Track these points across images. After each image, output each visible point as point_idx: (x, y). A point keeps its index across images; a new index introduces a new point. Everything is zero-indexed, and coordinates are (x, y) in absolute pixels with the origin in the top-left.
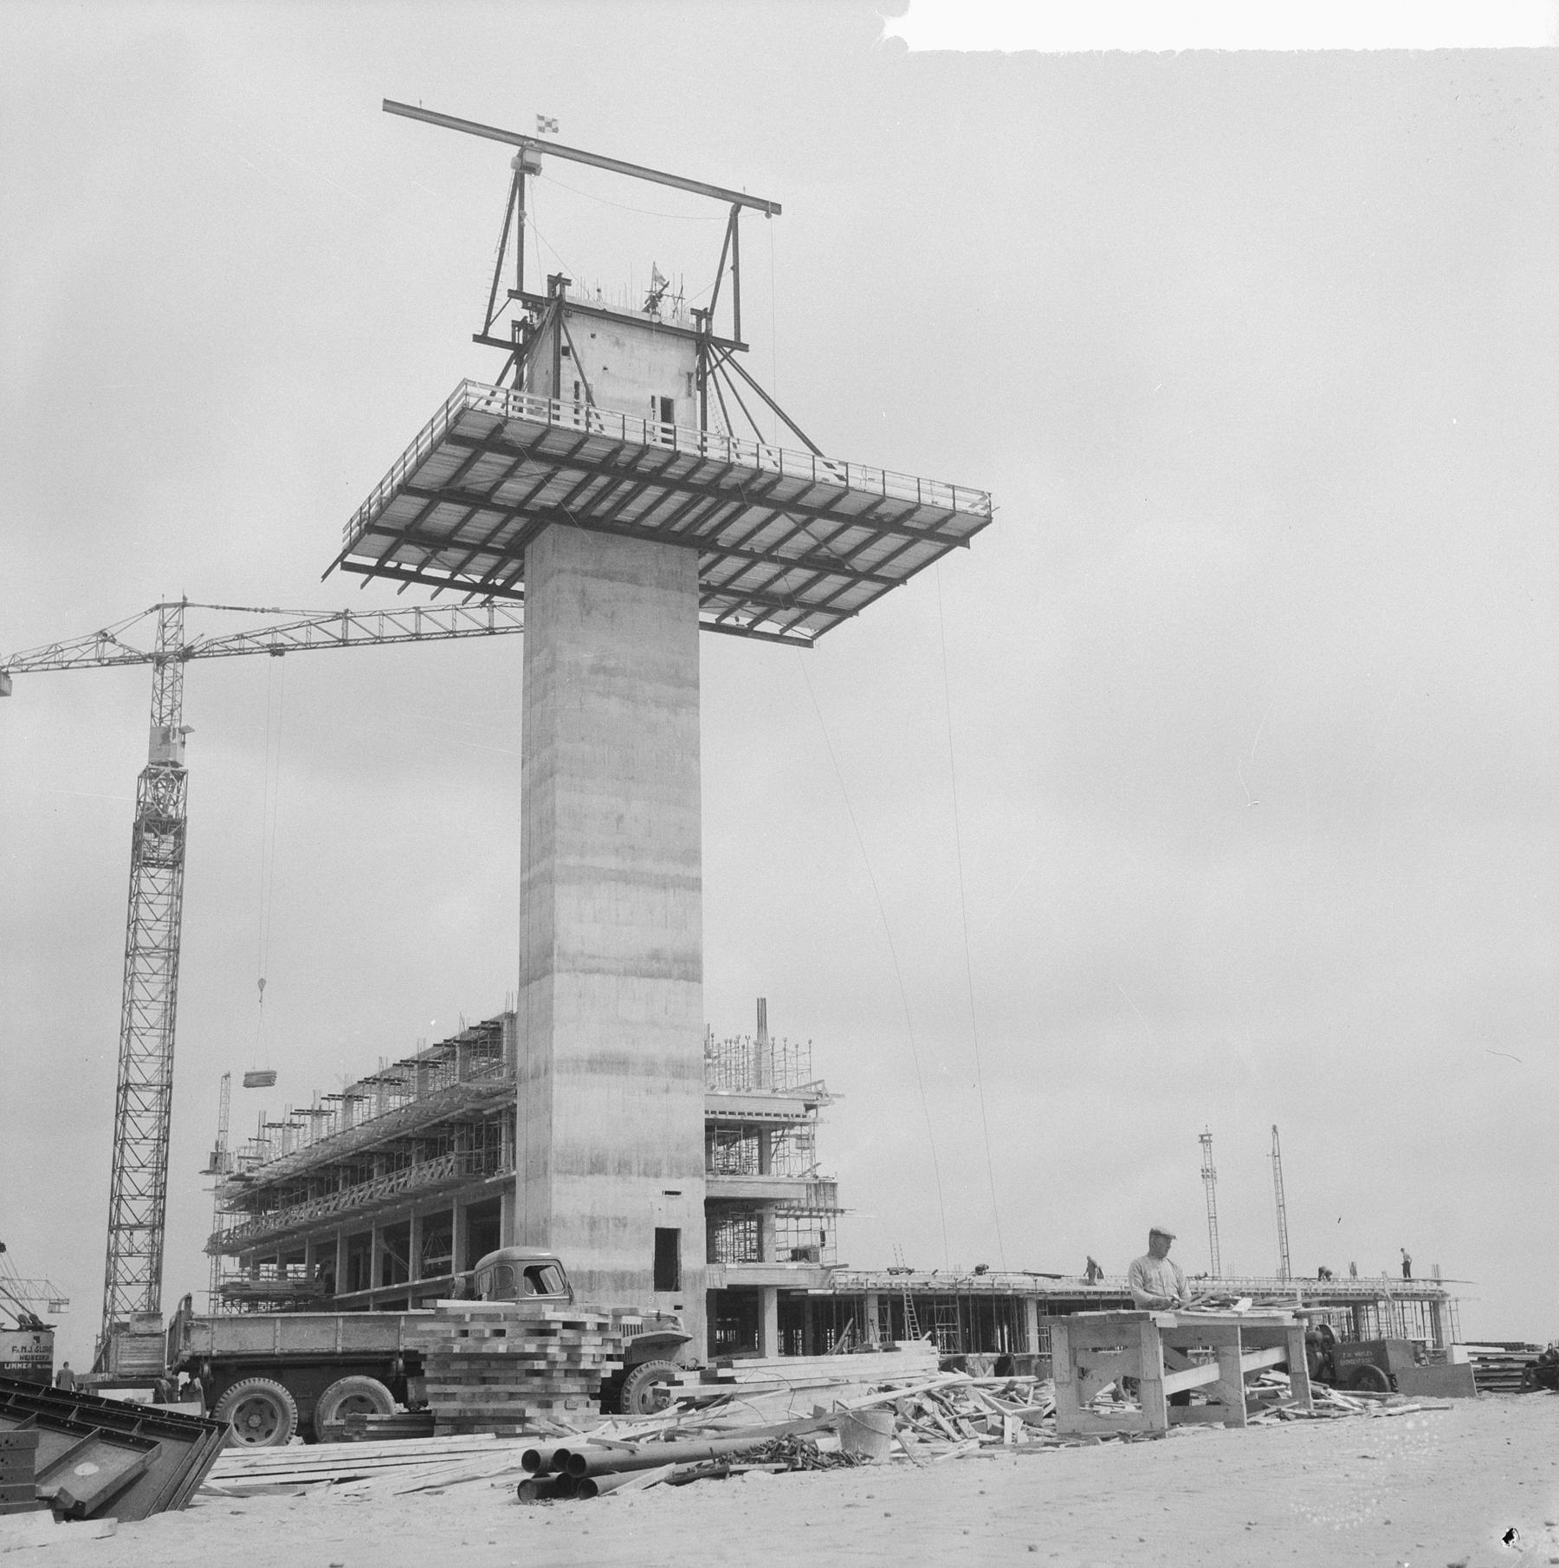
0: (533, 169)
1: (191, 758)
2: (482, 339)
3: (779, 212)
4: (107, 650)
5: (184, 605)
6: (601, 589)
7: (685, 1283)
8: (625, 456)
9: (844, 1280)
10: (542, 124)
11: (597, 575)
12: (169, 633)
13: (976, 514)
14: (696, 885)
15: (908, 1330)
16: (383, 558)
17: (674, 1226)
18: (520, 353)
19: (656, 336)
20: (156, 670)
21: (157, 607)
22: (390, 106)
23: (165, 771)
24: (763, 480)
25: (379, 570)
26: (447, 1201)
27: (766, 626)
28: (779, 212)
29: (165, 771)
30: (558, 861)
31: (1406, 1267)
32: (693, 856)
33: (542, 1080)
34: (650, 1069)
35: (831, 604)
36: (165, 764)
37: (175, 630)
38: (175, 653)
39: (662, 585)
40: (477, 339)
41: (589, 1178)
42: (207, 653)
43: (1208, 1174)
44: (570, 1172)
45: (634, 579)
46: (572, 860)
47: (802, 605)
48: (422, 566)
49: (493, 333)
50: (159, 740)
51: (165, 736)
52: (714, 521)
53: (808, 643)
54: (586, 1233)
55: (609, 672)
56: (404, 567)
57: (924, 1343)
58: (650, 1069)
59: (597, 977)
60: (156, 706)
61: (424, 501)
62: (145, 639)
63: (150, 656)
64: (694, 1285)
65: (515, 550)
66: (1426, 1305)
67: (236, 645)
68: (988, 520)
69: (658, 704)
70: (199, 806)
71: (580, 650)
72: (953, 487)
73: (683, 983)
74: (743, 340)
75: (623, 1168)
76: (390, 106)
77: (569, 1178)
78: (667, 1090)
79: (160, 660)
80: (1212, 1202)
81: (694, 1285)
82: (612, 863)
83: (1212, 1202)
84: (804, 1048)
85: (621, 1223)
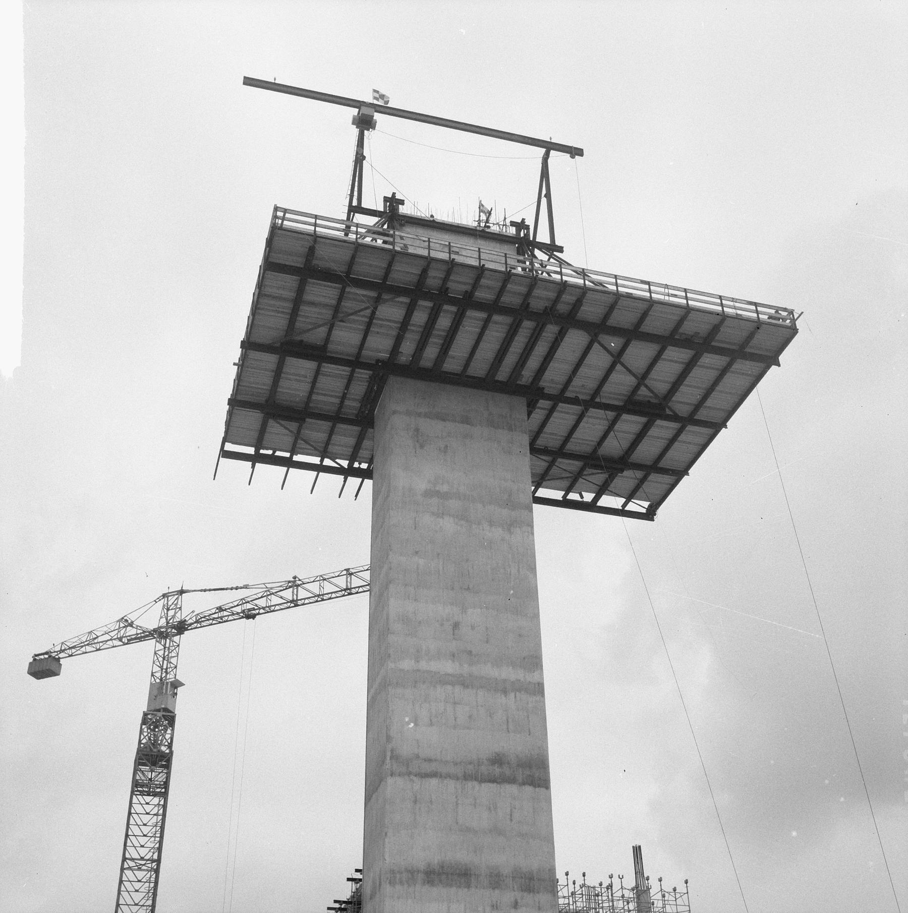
1: (182, 706)
3: (582, 155)
4: (129, 634)
8: (434, 279)
10: (377, 96)
11: (427, 416)
12: (171, 613)
15: (533, 677)
22: (249, 82)
23: (159, 717)
24: (569, 297)
27: (606, 501)
28: (582, 155)
29: (159, 717)
32: (534, 662)
34: (496, 880)
36: (159, 710)
39: (492, 424)
45: (466, 420)
46: (407, 664)
47: (637, 466)
48: (293, 452)
52: (533, 363)
55: (444, 496)
56: (278, 453)
57: (561, 312)
58: (496, 880)
59: (434, 781)
61: (599, 504)
62: (153, 620)
65: (366, 420)
69: (491, 523)
70: (184, 742)
73: (528, 789)
74: (558, 243)
79: (160, 634)
82: (448, 667)
84: (681, 888)
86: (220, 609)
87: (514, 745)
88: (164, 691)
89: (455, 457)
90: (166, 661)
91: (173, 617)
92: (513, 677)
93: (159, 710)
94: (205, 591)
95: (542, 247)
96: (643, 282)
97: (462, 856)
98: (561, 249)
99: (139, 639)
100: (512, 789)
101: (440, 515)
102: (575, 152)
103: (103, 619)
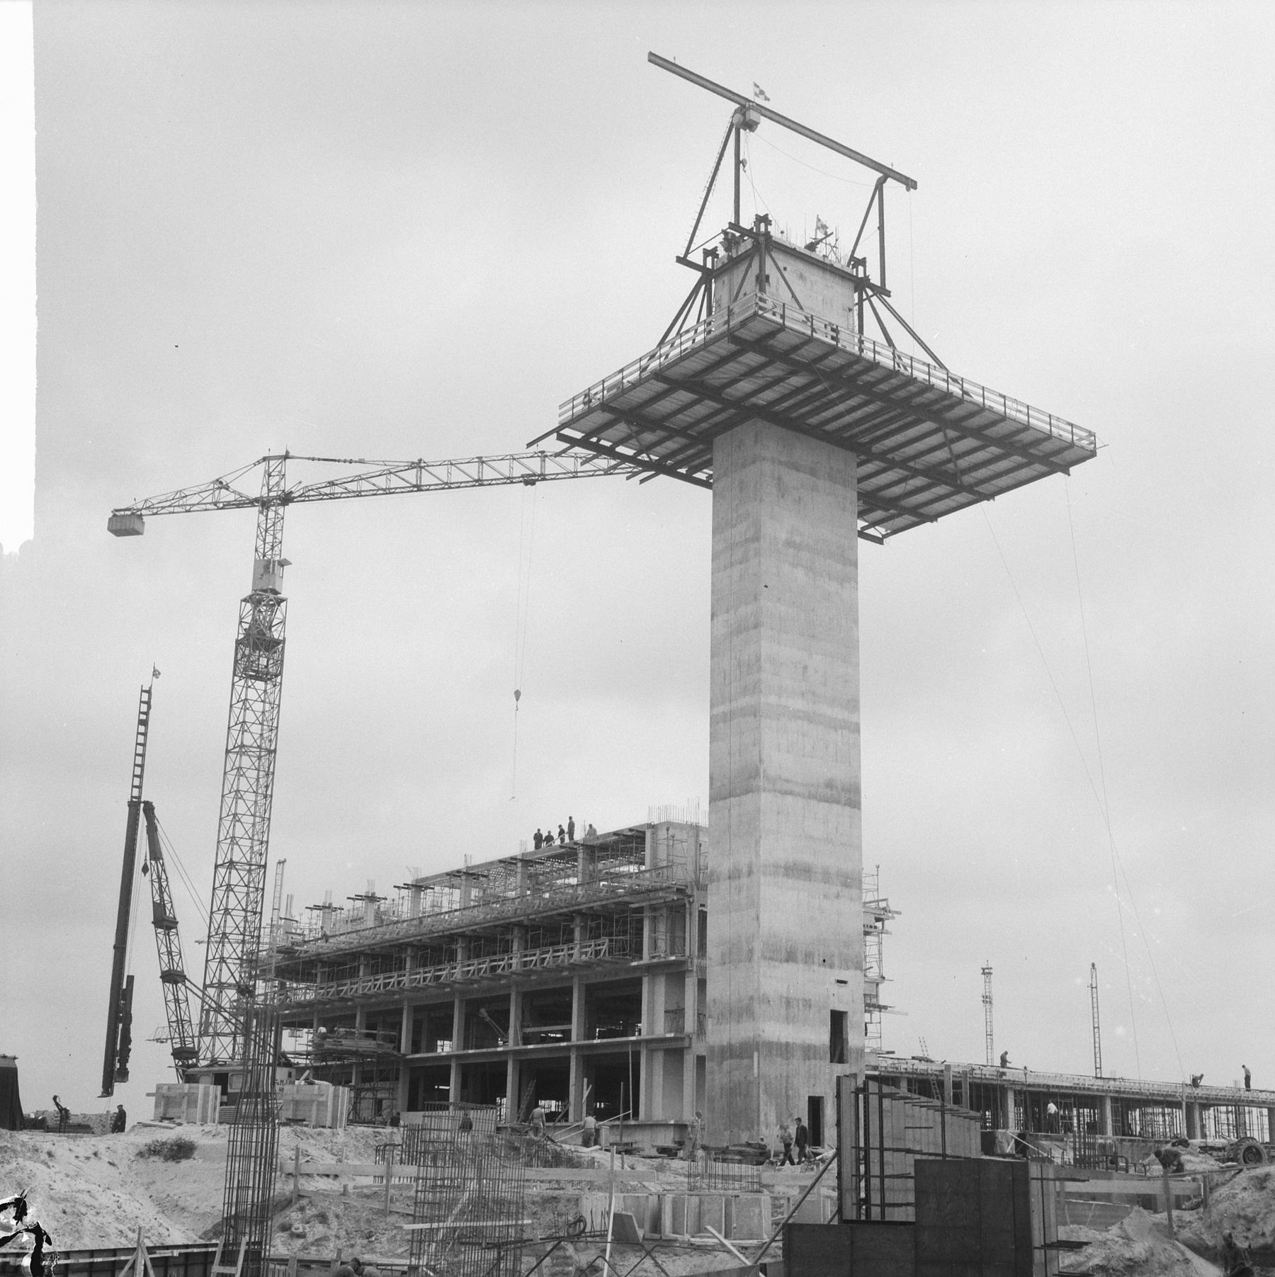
0: (751, 126)
1: (288, 585)
2: (682, 260)
3: (915, 188)
5: (286, 457)
6: (791, 477)
7: (851, 1057)
9: (884, 1064)
12: (273, 481)
13: (1082, 448)
14: (856, 729)
15: (854, 718)
16: (589, 435)
17: (842, 1009)
18: (708, 276)
19: (828, 276)
20: (261, 512)
21: (264, 459)
22: (654, 59)
23: (265, 596)
25: (583, 443)
26: (570, 978)
28: (915, 188)
29: (265, 596)
30: (763, 700)
31: (1248, 1079)
32: (853, 705)
33: (744, 880)
34: (827, 877)
35: (922, 511)
37: (277, 479)
38: (278, 497)
39: (831, 478)
40: (679, 260)
41: (785, 965)
42: (304, 497)
43: (987, 1000)
44: (771, 959)
45: (813, 473)
46: (773, 699)
49: (690, 258)
50: (262, 571)
51: (268, 567)
53: (880, 541)
54: (783, 1012)
55: (797, 547)
56: (603, 442)
58: (827, 877)
59: (789, 799)
60: (260, 543)
61: (665, 386)
63: (256, 500)
64: (857, 1059)
66: (1265, 1111)
67: (327, 490)
68: (1093, 454)
70: (296, 627)
71: (779, 524)
72: (1072, 425)
73: (848, 808)
75: (808, 958)
76: (654, 59)
77: (773, 963)
78: (838, 896)
79: (264, 504)
80: (989, 1023)
81: (857, 1059)
82: (799, 704)
83: (989, 1023)
85: (808, 1004)
86: (332, 484)
87: (839, 773)
88: (268, 567)
89: (803, 505)
90: (269, 533)
91: (277, 484)
92: (840, 717)
93: (265, 591)
94: (313, 459)
95: (872, 287)
96: (1001, 395)
97: (806, 858)
98: (888, 294)
99: (239, 505)
100: (836, 808)
101: (794, 565)
102: (910, 184)
103: (197, 477)
